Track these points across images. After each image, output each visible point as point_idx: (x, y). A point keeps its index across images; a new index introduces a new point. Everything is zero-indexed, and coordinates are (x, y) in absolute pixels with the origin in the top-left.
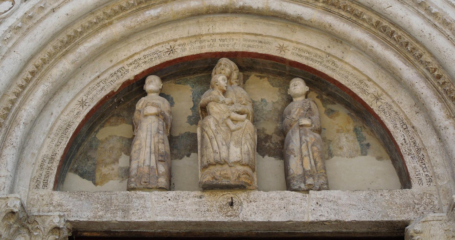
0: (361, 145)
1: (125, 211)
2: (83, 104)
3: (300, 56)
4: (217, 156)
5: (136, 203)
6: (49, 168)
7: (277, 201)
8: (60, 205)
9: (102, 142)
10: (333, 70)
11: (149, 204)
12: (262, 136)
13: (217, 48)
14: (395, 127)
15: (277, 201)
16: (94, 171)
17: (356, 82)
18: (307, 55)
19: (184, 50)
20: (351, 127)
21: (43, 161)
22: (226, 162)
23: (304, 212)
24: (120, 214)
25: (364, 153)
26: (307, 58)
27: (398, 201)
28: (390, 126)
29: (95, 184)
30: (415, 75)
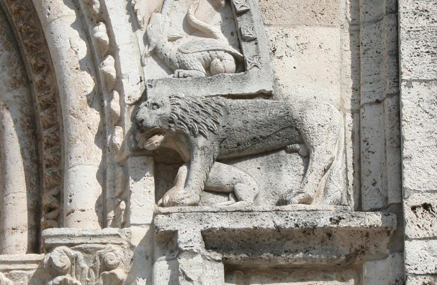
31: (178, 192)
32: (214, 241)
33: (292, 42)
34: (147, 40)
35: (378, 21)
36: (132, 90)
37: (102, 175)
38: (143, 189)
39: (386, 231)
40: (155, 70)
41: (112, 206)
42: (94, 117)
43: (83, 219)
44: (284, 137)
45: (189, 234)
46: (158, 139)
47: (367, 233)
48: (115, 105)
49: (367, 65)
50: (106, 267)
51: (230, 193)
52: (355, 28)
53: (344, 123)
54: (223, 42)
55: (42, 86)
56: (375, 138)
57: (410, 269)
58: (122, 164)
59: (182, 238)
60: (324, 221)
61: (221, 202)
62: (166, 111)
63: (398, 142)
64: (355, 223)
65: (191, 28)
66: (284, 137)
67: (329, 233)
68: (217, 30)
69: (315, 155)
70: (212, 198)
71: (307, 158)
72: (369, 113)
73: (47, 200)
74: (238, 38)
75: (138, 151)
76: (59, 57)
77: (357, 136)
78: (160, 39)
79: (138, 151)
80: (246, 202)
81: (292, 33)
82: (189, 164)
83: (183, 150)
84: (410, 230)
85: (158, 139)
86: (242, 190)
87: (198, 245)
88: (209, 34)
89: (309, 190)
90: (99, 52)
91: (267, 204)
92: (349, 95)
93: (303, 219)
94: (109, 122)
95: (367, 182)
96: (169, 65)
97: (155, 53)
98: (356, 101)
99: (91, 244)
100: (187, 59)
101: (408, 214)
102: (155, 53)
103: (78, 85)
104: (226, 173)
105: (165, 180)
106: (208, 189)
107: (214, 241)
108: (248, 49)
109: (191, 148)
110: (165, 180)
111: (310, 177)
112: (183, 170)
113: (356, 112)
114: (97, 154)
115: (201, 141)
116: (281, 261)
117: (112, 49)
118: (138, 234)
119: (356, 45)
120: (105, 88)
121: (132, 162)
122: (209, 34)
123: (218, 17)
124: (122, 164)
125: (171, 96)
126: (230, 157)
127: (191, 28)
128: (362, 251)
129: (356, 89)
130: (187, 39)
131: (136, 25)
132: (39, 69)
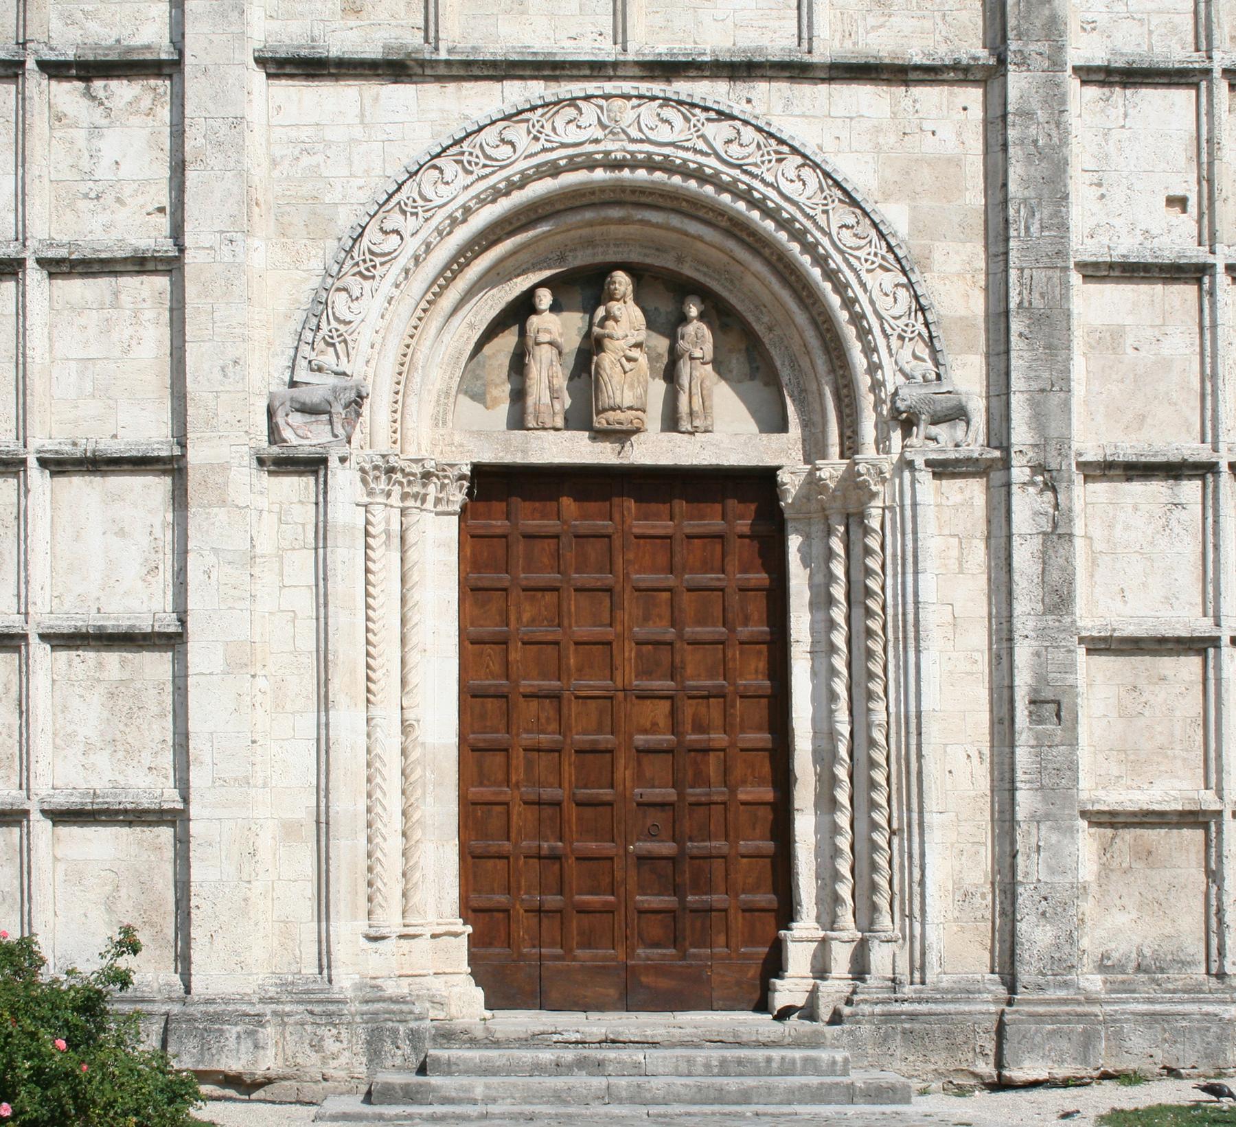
0: (751, 368)
1: (525, 452)
2: (472, 326)
3: (698, 270)
4: (612, 402)
5: (535, 444)
6: (446, 404)
7: (665, 444)
8: (461, 445)
9: (489, 357)
10: (731, 291)
11: (546, 445)
12: (654, 355)
13: (612, 257)
14: (783, 365)
15: (665, 444)
16: (484, 394)
17: (752, 307)
18: (705, 269)
19: (575, 258)
20: (743, 346)
21: (439, 396)
22: (620, 408)
23: (688, 455)
24: (519, 454)
25: (752, 378)
26: (705, 274)
27: (773, 446)
28: (778, 364)
29: (487, 408)
30: (806, 322)
31: (913, 440)
32: (929, 463)
33: (959, 362)
34: (896, 363)
35: (998, 354)
36: (891, 388)
37: (876, 426)
38: (896, 436)
39: (1001, 459)
40: (901, 380)
41: (882, 442)
42: (871, 397)
43: (869, 451)
44: (958, 414)
45: (919, 462)
46: (904, 415)
47: (993, 460)
48: (883, 395)
49: (993, 377)
50: (881, 473)
51: (935, 439)
52: (988, 355)
53: (982, 404)
54: (930, 364)
55: (843, 376)
56: (996, 412)
57: (1013, 481)
58: (886, 423)
59: (916, 463)
60: (976, 455)
61: (932, 444)
62: (908, 403)
63: (1008, 419)
64: (989, 456)
65: (916, 357)
66: (958, 414)
67: (977, 460)
68: (927, 357)
69: (972, 423)
70: (928, 442)
71: (968, 423)
72: (994, 400)
73: (849, 433)
74: (937, 364)
75: (895, 418)
76: (855, 367)
77: (988, 410)
78: (902, 363)
79: (895, 418)
80: (942, 444)
81: (959, 357)
82: (918, 426)
83: (915, 420)
84: (1014, 463)
85: (904, 415)
86: (940, 438)
87: (923, 466)
88: (923, 360)
89: (969, 440)
90: (873, 368)
91: (950, 446)
92: (984, 389)
93: (967, 454)
94: (878, 403)
95: (993, 433)
96: (907, 377)
97: (901, 370)
98: (988, 392)
99: (875, 462)
100: (915, 374)
101: (1013, 455)
102: (901, 370)
103: (864, 381)
104: (934, 430)
105: (907, 434)
106: (927, 438)
107: (929, 463)
108: (942, 370)
109: (919, 420)
110: (907, 434)
111: (970, 434)
112: (915, 429)
113: (988, 397)
114: (874, 416)
115: (923, 417)
116: (956, 470)
117: (879, 366)
118: (895, 457)
119: (988, 364)
120: (876, 386)
121: (892, 423)
122: (923, 360)
123: (927, 350)
124: (886, 423)
125: (910, 396)
126: (934, 423)
127: (916, 357)
128: (990, 467)
129: (988, 386)
130: (914, 362)
131: (891, 355)
132: (841, 367)
